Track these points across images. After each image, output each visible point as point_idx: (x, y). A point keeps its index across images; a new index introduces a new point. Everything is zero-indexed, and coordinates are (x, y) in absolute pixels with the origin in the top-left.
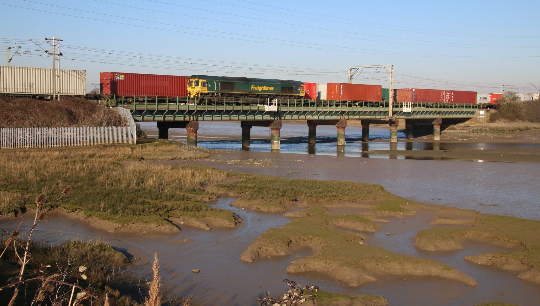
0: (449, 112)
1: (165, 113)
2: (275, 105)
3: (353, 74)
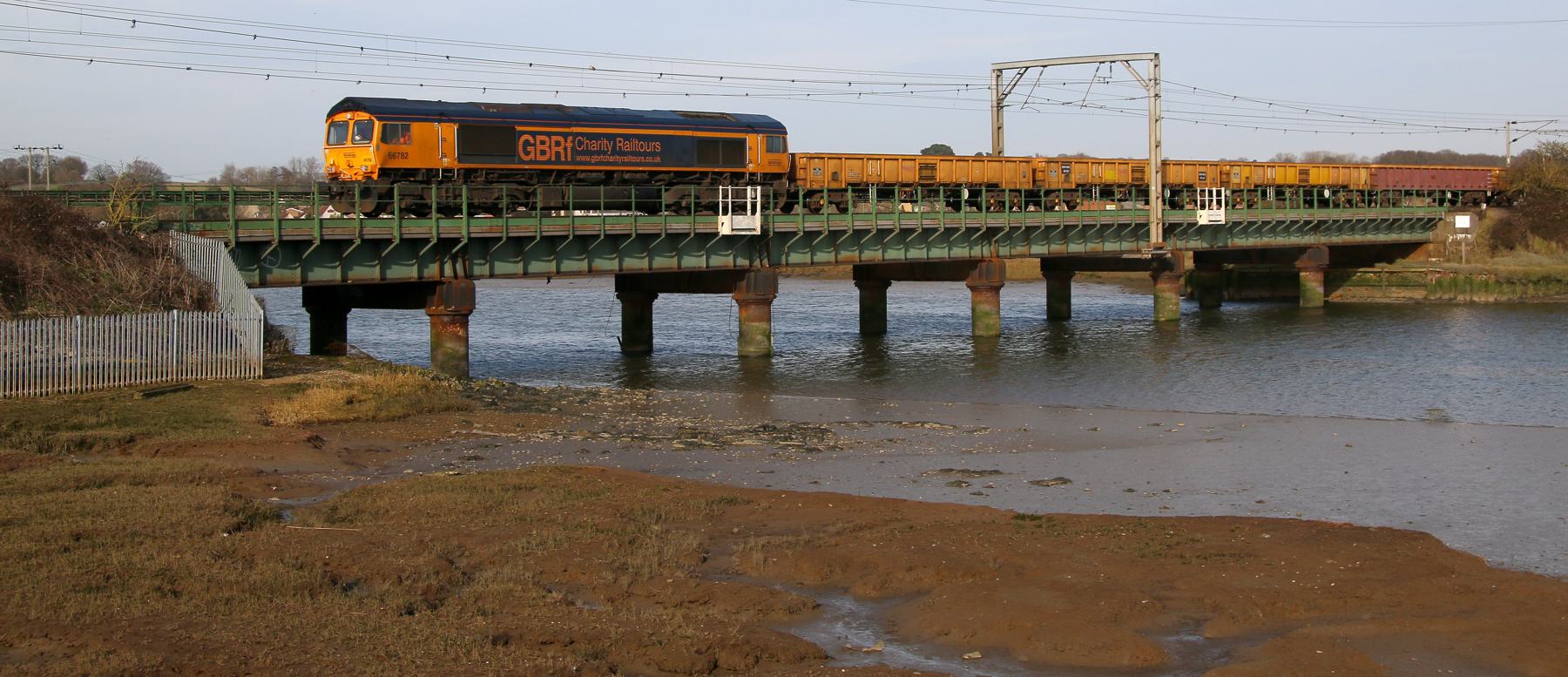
0: (1351, 221)
2: (753, 212)
3: (1008, 90)
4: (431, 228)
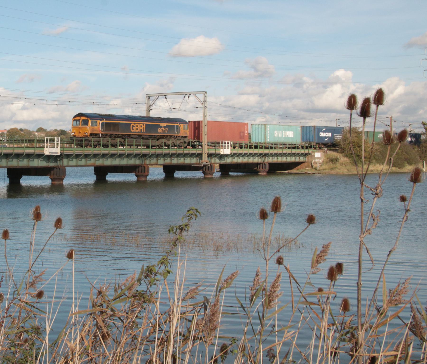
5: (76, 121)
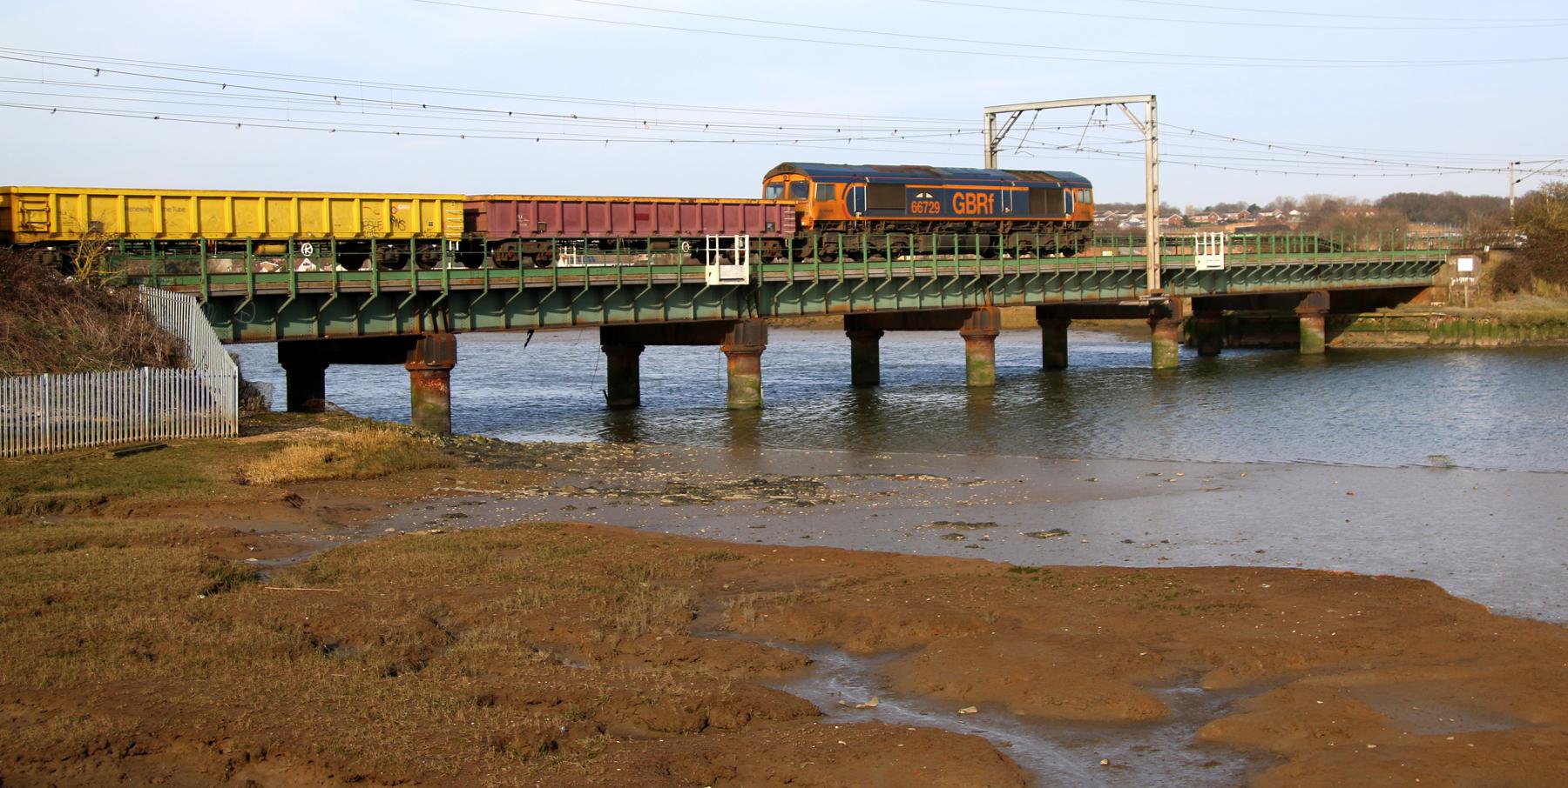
1: (782, 290)
2: (742, 261)
4: (410, 280)
5: (775, 186)
